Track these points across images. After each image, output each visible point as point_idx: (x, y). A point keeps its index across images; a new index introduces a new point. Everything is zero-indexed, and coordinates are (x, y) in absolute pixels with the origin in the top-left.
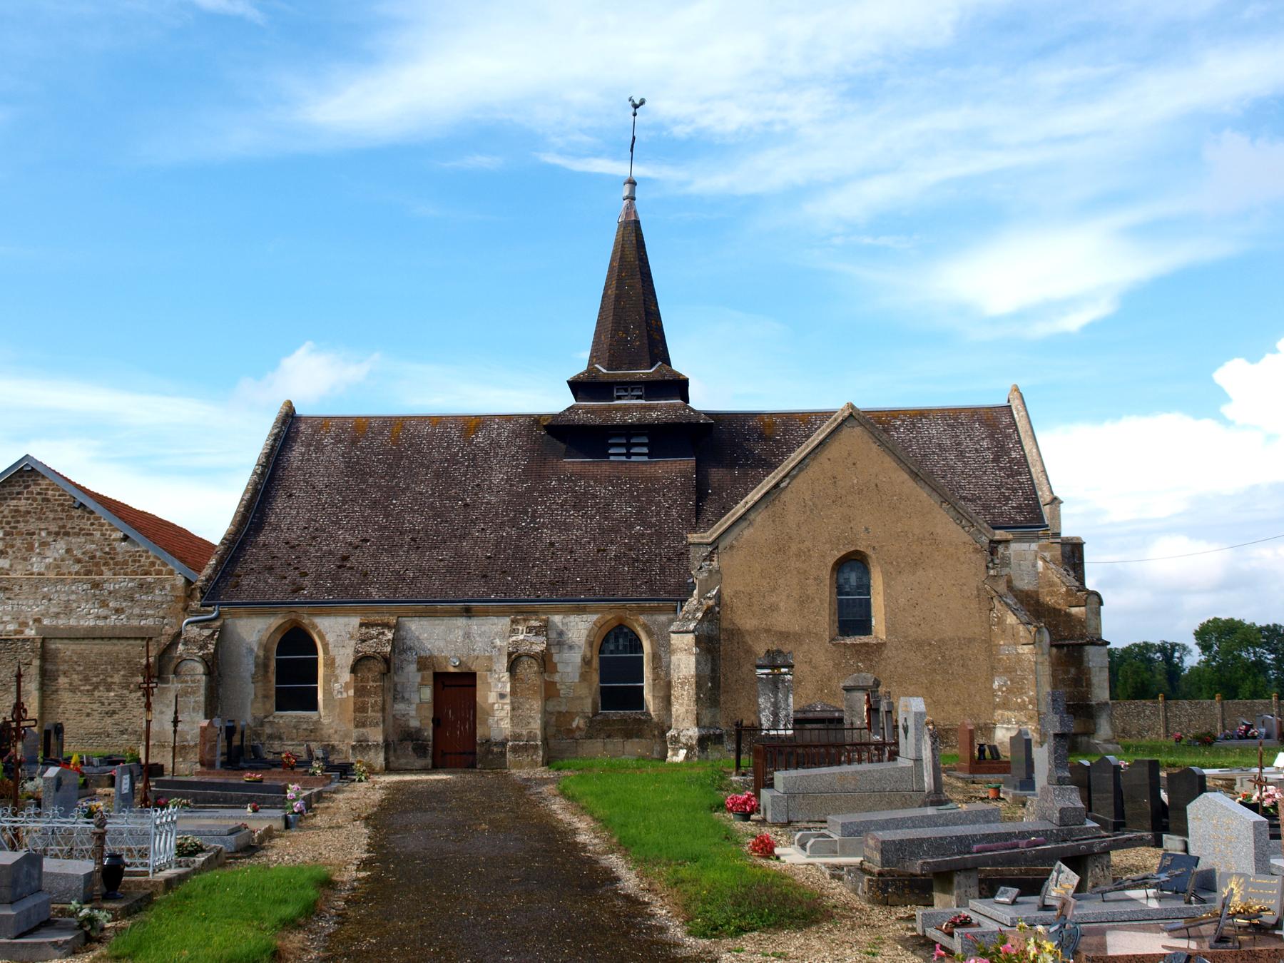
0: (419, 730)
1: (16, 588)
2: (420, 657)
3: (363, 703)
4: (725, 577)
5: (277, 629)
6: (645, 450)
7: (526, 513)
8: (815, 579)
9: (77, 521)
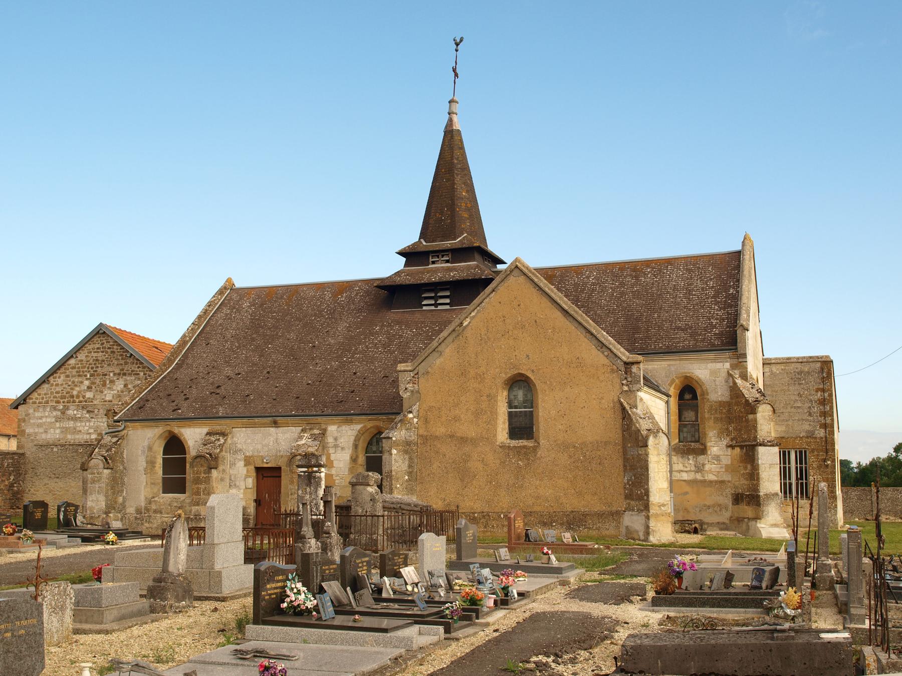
1: (96, 411)
2: (246, 457)
3: (198, 488)
4: (422, 396)
5: (357, 439)
6: (448, 301)
7: (349, 351)
8: (488, 396)
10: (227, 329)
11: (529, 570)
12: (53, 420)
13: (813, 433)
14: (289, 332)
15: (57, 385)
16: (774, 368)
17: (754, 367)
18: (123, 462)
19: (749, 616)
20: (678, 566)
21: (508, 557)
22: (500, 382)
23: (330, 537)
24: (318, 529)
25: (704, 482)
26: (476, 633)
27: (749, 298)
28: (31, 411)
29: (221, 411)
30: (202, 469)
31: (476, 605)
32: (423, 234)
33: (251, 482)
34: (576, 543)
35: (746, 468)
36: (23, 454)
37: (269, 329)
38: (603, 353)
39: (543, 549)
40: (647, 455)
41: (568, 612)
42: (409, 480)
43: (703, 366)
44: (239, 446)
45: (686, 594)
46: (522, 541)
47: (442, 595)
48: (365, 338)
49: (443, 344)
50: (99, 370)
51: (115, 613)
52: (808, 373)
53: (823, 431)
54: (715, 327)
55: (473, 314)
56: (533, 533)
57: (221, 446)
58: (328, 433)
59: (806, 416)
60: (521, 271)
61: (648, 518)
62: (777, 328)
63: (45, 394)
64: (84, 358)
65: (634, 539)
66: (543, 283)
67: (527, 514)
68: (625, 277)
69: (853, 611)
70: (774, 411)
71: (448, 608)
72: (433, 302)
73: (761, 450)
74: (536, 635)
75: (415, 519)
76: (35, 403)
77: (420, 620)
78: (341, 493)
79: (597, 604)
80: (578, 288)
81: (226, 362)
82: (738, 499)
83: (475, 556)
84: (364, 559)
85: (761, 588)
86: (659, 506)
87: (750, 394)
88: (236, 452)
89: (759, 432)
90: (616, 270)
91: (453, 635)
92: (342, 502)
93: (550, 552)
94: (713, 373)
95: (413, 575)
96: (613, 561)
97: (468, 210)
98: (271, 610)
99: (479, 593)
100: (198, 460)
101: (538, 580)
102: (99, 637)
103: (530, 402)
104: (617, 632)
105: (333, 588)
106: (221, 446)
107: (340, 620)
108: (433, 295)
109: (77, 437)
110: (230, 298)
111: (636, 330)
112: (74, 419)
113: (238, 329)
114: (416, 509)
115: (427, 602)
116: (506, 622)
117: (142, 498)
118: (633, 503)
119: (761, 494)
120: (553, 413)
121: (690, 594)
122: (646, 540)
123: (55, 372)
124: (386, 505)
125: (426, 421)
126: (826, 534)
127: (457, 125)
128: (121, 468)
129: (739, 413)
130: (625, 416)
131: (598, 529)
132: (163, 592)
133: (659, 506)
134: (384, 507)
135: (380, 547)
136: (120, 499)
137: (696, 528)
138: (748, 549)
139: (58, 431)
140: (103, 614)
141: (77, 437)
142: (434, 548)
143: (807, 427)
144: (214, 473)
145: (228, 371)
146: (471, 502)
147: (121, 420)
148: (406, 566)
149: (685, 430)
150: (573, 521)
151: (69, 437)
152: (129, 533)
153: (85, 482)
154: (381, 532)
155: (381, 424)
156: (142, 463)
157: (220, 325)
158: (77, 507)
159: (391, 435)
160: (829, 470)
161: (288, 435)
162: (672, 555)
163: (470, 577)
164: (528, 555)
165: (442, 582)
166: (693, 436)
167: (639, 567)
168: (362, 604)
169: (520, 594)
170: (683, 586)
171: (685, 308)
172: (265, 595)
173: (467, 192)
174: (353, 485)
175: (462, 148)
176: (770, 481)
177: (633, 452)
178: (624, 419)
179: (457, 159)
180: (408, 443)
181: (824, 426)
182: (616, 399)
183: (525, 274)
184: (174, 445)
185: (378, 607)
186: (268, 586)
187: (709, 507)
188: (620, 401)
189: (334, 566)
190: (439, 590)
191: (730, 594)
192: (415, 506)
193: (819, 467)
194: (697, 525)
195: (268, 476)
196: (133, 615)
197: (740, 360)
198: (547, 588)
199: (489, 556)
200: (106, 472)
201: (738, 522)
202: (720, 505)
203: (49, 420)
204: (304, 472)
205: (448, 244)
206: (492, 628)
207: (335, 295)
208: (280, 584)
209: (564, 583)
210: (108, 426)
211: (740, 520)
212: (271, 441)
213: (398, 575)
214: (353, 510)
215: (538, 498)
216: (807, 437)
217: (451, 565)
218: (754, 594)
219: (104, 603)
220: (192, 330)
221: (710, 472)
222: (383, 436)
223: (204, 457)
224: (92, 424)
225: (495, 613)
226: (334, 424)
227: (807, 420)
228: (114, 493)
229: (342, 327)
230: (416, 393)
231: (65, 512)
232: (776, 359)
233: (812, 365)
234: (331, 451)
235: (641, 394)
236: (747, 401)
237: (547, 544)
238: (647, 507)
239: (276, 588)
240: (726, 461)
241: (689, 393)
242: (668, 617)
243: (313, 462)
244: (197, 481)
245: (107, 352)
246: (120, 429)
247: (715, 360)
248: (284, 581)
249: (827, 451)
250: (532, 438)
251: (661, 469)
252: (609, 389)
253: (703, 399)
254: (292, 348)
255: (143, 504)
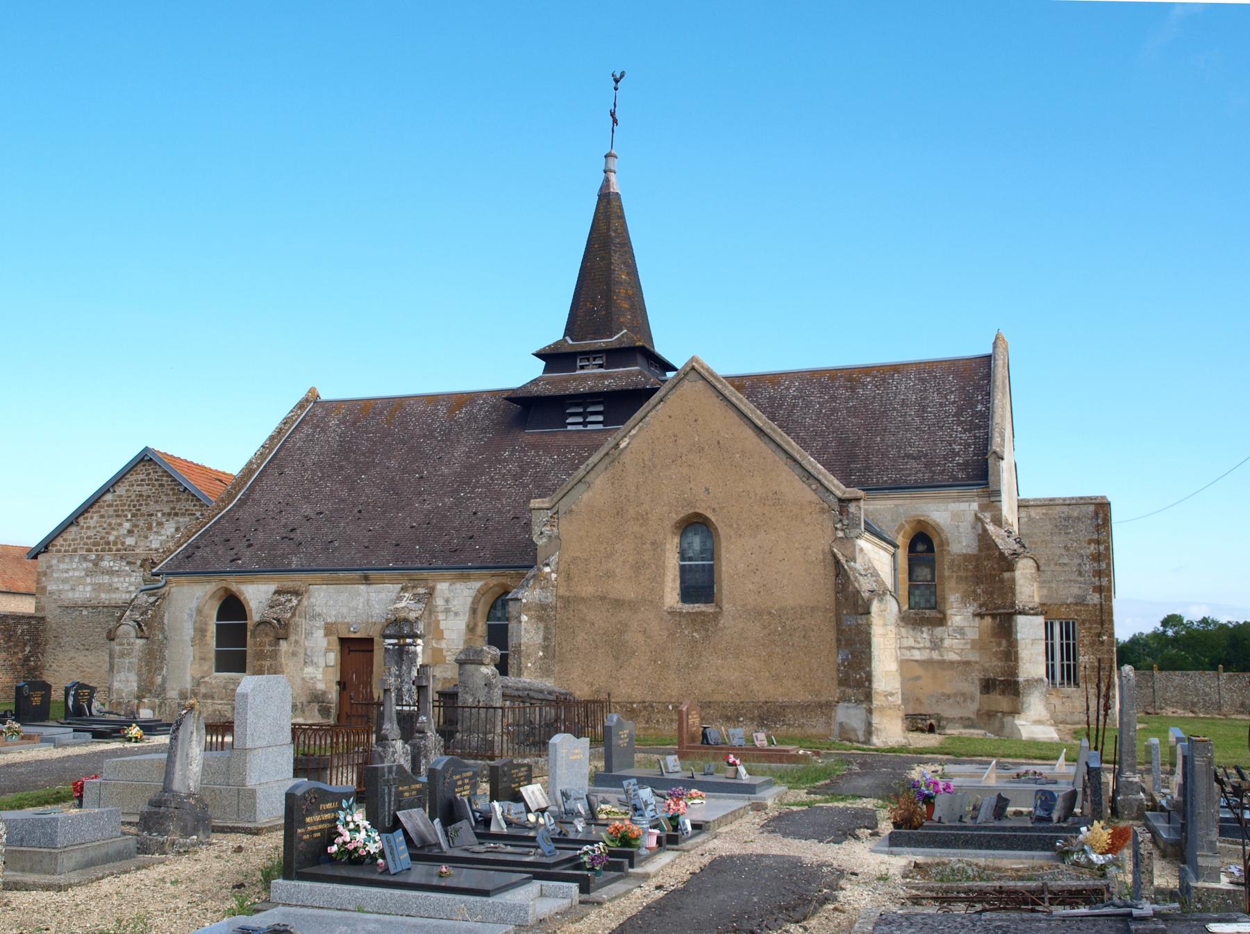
0: (324, 693)
5: (476, 601)
7: (468, 484)
8: (653, 544)
9: (184, 503)
10: (307, 454)
11: (706, 787)
12: (83, 574)
13: (1084, 598)
14: (389, 459)
15: (88, 528)
16: (1034, 513)
17: (1009, 510)
18: (162, 630)
19: (1037, 862)
20: (927, 786)
21: (678, 769)
22: (668, 524)
23: (425, 738)
24: (408, 726)
25: (942, 663)
26: (629, 891)
27: (1003, 417)
28: (54, 562)
29: (295, 562)
30: (267, 640)
31: (630, 845)
32: (569, 331)
33: (333, 658)
34: (773, 747)
35: (999, 644)
36: (43, 618)
37: (363, 454)
38: (810, 486)
39: (727, 757)
40: (869, 625)
41: (767, 856)
42: (545, 657)
43: (942, 506)
44: (318, 609)
45: (939, 828)
46: (698, 744)
47: (580, 829)
48: (489, 467)
49: (592, 473)
50: (143, 508)
51: (77, 857)
52: (1078, 518)
53: (1097, 595)
54: (958, 454)
55: (633, 432)
56: (713, 734)
57: (294, 609)
58: (437, 593)
59: (1074, 576)
60: (699, 374)
61: (870, 711)
62: (1038, 463)
63: (73, 540)
64: (123, 493)
65: (850, 741)
66: (729, 391)
67: (705, 705)
68: (837, 389)
69: (1201, 862)
70: (1038, 568)
71: (586, 853)
72: (581, 420)
73: (1021, 620)
74: (721, 897)
75: (550, 712)
76: (59, 551)
77: (542, 872)
78: (443, 675)
79: (808, 842)
80: (777, 402)
81: (305, 497)
82: (988, 686)
83: (631, 766)
84: (465, 775)
85: (1050, 820)
86: (886, 696)
87: (1006, 545)
88: (313, 617)
89: (1018, 596)
90: (825, 379)
91: (594, 895)
92: (448, 687)
93: (738, 762)
94: (955, 516)
95: (540, 797)
96: (825, 773)
97: (628, 298)
98: (311, 856)
99: (635, 828)
100: (262, 627)
101: (722, 802)
102: (44, 897)
103: (711, 552)
104: (842, 889)
105: (415, 819)
106: (294, 609)
107: (420, 872)
108: (581, 410)
109: (114, 596)
110: (313, 413)
111: (852, 457)
112: (111, 572)
113: (322, 454)
114: (550, 697)
115: (554, 840)
116: (674, 872)
117: (189, 679)
118: (849, 691)
119: (1021, 679)
120: (741, 567)
121: (945, 828)
122: (868, 742)
123: (86, 511)
124: (508, 692)
125: (569, 577)
126: (1132, 739)
127: (615, 187)
128: (161, 637)
129: (991, 570)
130: (839, 571)
131: (801, 726)
132: (164, 821)
133: (886, 696)
134: (504, 695)
135: (497, 752)
136: (159, 680)
137: (931, 725)
138: (1009, 756)
139: (89, 588)
140: (56, 859)
141: (114, 596)
142: (571, 756)
143: (1075, 590)
144: (284, 645)
145: (307, 509)
146: (627, 689)
147: (161, 573)
148: (530, 783)
149: (917, 592)
150: (767, 715)
151: (103, 596)
152: (163, 725)
153: (111, 657)
154: (499, 730)
155: (508, 581)
156: (188, 631)
157: (299, 449)
158: (93, 690)
159: (520, 596)
160: (1105, 648)
161: (383, 595)
162: (908, 764)
163: (623, 797)
164: (706, 766)
165: (581, 807)
166: (928, 601)
167: (864, 783)
168: (462, 845)
169: (694, 826)
170: (935, 817)
171: (917, 430)
172: (303, 834)
173: (628, 274)
174: (461, 663)
175: (621, 217)
176: (1032, 662)
177: (849, 621)
178: (837, 576)
179: (615, 231)
180: (543, 607)
181: (1099, 589)
182: (827, 549)
183: (704, 378)
184: (232, 607)
185: (481, 848)
186: (308, 820)
187: (949, 697)
188: (832, 552)
189: (418, 786)
190: (576, 821)
191: (1004, 829)
192: (550, 693)
193: (1092, 644)
194: (933, 721)
195: (355, 649)
196: (108, 859)
197: (993, 499)
198: (735, 815)
199: (651, 764)
200: (140, 642)
201: (987, 717)
202: (963, 694)
203: (77, 574)
204: (394, 645)
205: (602, 343)
206: (654, 882)
207: (451, 410)
208: (327, 816)
209: (759, 807)
210: (144, 581)
211: (990, 715)
212: (359, 603)
213: (518, 798)
214: (460, 698)
215: (720, 682)
216: (1076, 604)
217: (597, 779)
218: (1040, 830)
219: (61, 840)
220: (261, 455)
221: (951, 649)
222: (509, 596)
223: (270, 623)
224: (133, 579)
225: (658, 857)
226: (445, 580)
227: (1075, 581)
228: (149, 671)
229: (459, 452)
230: (555, 540)
231: (75, 696)
232: (1035, 500)
233: (1084, 508)
234: (441, 617)
235: (861, 543)
236: (1002, 554)
237: (733, 749)
238: (868, 697)
239: (322, 822)
240: (973, 634)
241: (923, 543)
242: (916, 865)
243: (406, 630)
244: (260, 655)
245: (154, 486)
246: (160, 584)
247: (958, 499)
248: (335, 810)
249: (1102, 624)
250: (712, 602)
251: (890, 646)
252: (817, 535)
253: (942, 551)
254: (392, 480)
255: (189, 686)
